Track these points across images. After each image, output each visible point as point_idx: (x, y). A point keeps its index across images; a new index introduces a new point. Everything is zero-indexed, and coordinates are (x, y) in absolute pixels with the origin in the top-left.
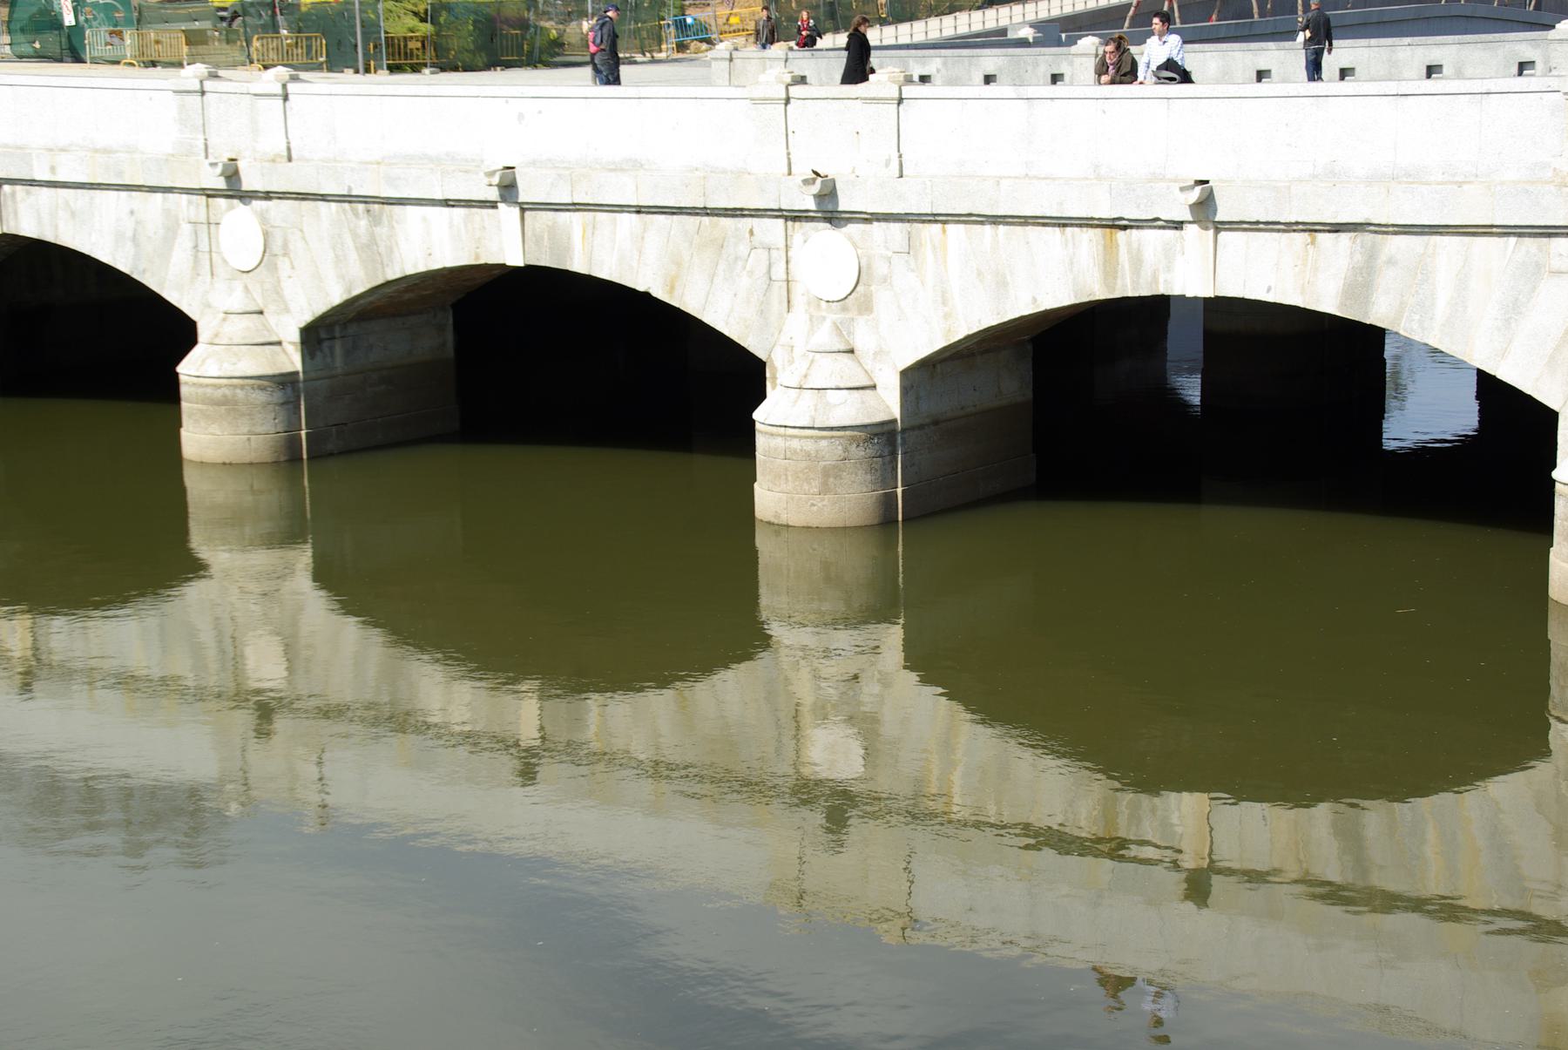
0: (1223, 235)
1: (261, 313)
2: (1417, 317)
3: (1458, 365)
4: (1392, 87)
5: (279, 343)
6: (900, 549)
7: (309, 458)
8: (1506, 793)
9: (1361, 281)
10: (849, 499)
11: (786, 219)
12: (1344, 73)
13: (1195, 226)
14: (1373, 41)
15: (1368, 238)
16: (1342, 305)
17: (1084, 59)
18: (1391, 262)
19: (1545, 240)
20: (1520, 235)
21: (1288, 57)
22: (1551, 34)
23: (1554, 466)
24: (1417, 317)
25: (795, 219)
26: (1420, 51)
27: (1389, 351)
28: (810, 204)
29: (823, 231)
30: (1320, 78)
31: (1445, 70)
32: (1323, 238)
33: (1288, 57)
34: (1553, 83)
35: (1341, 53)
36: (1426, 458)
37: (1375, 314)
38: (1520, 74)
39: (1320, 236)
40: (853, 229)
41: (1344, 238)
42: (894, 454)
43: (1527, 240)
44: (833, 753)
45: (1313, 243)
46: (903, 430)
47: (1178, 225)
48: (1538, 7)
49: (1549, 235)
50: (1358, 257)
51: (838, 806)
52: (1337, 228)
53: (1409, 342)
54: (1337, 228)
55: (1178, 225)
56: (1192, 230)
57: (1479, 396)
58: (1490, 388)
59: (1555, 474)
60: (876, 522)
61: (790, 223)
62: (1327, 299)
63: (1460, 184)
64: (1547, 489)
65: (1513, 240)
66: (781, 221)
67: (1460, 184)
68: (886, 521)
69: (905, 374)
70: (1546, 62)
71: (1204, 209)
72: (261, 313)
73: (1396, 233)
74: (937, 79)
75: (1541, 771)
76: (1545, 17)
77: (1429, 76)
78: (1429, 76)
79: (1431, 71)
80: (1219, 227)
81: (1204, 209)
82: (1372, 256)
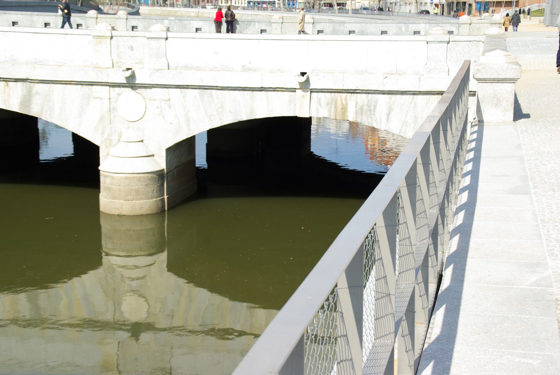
0: (313, 94)
1: (142, 141)
2: (48, 113)
3: (67, 130)
4: (32, 30)
5: (153, 155)
6: (166, 223)
7: (168, 209)
8: (89, 280)
9: (27, 100)
10: (144, 203)
11: (110, 86)
12: (78, 26)
13: (300, 90)
14: (24, 13)
15: (28, 84)
16: (20, 108)
17: (465, 26)
18: (37, 93)
19: (90, 87)
20: (82, 85)
21: (56, 18)
22: (86, 15)
23: (99, 165)
24: (48, 113)
25: (113, 86)
26: (41, 17)
27: (40, 126)
28: (124, 81)
29: (128, 91)
30: (220, 32)
31: (51, 25)
32: (11, 84)
33: (56, 18)
34: (88, 32)
35: (75, 18)
36: (59, 162)
37: (33, 112)
38: (78, 28)
39: (10, 83)
40: (139, 90)
41: (19, 84)
42: (162, 185)
43: (84, 86)
44: (133, 309)
45: (7, 85)
46: (167, 173)
47: (293, 90)
48: (82, 5)
49: (92, 85)
50: (25, 91)
51: (136, 329)
52: (16, 80)
53: (47, 122)
54: (16, 80)
55: (293, 90)
56: (299, 92)
57: (73, 140)
58: (77, 139)
59: (100, 168)
60: (154, 212)
61: (111, 88)
62: (15, 107)
63: (60, 66)
64: (97, 173)
65: (80, 86)
66: (108, 87)
67: (60, 66)
68: (162, 211)
69: (169, 150)
70: (86, 24)
71: (305, 85)
72: (142, 141)
73: (37, 83)
74: (140, 28)
75: (100, 272)
76: (84, 9)
77: (46, 27)
78: (46, 27)
79: (46, 25)
80: (312, 91)
81: (305, 85)
82: (30, 91)
